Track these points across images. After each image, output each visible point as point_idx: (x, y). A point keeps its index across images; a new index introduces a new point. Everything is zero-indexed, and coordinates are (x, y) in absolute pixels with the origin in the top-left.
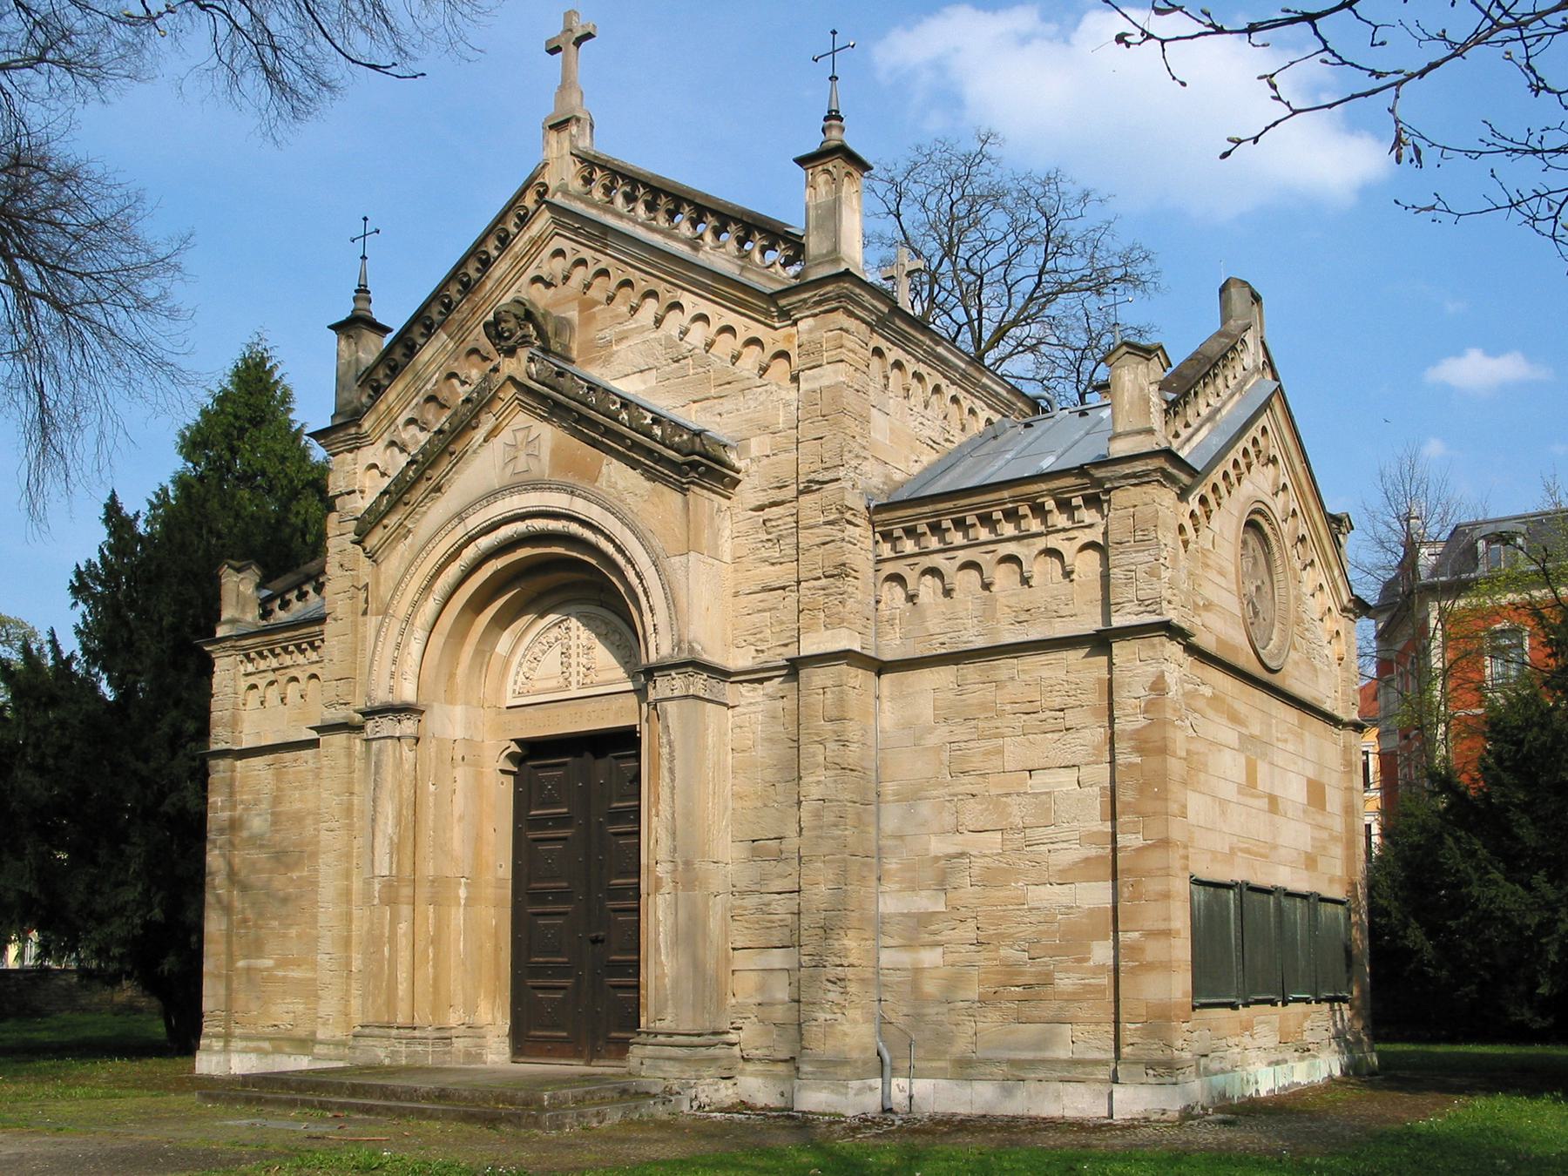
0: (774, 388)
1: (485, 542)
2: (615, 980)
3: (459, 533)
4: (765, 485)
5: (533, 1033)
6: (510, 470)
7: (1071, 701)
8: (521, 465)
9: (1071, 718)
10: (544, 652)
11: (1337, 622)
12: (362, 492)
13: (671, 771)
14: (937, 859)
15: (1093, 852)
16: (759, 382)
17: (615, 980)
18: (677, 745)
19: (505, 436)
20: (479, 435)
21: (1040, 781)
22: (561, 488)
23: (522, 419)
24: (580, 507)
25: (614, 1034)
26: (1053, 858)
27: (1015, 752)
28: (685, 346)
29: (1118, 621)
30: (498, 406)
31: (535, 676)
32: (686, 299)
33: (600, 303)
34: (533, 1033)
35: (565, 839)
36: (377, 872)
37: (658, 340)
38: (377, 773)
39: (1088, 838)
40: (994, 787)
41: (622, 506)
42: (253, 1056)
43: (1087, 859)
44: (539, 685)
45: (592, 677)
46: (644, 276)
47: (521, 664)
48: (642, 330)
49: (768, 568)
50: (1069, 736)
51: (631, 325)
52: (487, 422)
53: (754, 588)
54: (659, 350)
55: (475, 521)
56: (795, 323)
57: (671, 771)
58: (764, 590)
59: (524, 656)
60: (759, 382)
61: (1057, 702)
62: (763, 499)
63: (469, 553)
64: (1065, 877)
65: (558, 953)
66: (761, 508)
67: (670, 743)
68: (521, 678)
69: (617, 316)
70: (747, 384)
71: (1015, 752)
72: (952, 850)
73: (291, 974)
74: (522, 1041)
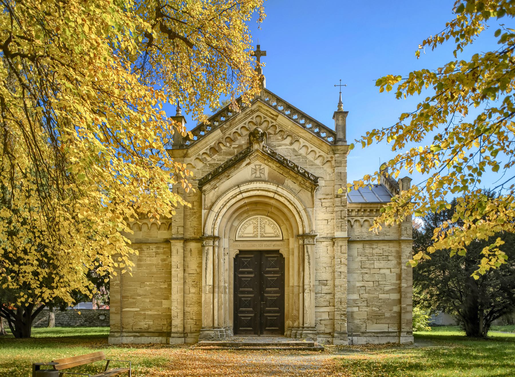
7: (390, 254)
8: (258, 175)
9: (390, 258)
11: (160, 232)
13: (309, 262)
14: (358, 287)
15: (394, 287)
16: (321, 167)
18: (311, 256)
19: (252, 166)
20: (244, 164)
21: (382, 271)
25: (267, 328)
26: (385, 288)
27: (377, 265)
29: (402, 238)
34: (267, 328)
36: (207, 284)
37: (291, 149)
38: (207, 255)
39: (394, 284)
40: (373, 271)
41: (287, 193)
42: (132, 338)
43: (392, 289)
48: (286, 145)
50: (389, 262)
52: (247, 161)
54: (291, 152)
55: (243, 188)
57: (309, 262)
60: (321, 167)
61: (387, 254)
64: (388, 292)
67: (309, 255)
69: (278, 139)
71: (377, 265)
72: (361, 285)
73: (147, 313)
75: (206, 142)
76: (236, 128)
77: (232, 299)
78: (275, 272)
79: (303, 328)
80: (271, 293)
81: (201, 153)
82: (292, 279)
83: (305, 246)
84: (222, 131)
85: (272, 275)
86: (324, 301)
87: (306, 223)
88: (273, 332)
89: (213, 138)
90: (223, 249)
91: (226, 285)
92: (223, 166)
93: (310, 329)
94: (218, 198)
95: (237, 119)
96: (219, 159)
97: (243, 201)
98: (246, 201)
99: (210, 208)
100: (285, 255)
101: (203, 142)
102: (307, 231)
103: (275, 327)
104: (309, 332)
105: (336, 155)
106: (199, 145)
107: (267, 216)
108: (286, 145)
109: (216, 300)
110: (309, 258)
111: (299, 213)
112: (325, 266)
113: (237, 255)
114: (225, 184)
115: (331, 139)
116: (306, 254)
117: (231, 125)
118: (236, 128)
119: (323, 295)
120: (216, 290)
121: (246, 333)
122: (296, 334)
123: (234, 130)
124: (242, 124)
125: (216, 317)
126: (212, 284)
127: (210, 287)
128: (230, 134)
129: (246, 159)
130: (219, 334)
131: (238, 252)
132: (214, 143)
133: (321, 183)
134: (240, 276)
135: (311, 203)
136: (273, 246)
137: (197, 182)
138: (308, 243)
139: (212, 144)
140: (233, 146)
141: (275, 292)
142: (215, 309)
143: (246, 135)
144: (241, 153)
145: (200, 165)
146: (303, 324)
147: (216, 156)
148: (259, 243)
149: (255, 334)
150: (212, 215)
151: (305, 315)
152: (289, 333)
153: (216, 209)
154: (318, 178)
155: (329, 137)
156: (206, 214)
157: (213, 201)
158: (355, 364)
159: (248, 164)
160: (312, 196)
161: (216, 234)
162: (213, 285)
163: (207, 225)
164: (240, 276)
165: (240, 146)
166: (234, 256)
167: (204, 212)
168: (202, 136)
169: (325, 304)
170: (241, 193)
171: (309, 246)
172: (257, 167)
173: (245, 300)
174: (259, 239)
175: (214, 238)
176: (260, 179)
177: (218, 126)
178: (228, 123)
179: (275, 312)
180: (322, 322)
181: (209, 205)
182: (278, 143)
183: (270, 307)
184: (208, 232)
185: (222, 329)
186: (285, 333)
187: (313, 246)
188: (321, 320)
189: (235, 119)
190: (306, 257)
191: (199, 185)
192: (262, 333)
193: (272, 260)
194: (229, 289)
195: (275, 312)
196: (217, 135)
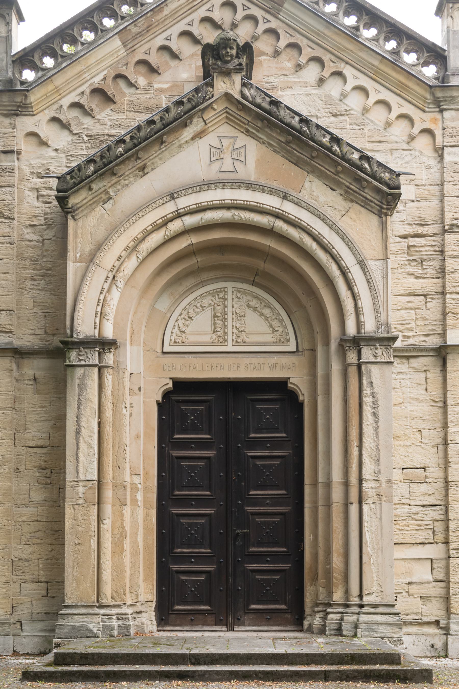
0: (417, 154)
1: (190, 221)
2: (255, 566)
3: (169, 208)
4: (410, 220)
5: (176, 608)
6: (211, 167)
8: (228, 165)
10: (197, 314)
12: (19, 153)
16: (406, 147)
17: (255, 566)
18: (380, 397)
19: (211, 139)
20: (188, 133)
22: (272, 192)
23: (226, 130)
24: (289, 208)
28: (342, 108)
30: (209, 115)
31: (188, 331)
32: (348, 71)
33: (267, 54)
35: (208, 458)
41: (318, 209)
44: (192, 338)
45: (243, 337)
46: (310, 44)
47: (177, 320)
48: (305, 85)
49: (412, 280)
51: (293, 79)
52: (197, 125)
53: (403, 292)
54: (320, 104)
55: (184, 202)
56: (441, 111)
57: (375, 415)
58: (410, 295)
59: (181, 314)
60: (406, 147)
62: (410, 230)
63: (176, 226)
65: (201, 545)
66: (405, 237)
67: (373, 395)
68: (176, 330)
69: (282, 69)
70: (395, 146)
74: (167, 612)
75: (80, 74)
76: (165, 35)
77: (154, 520)
78: (276, 444)
79: (361, 606)
80: (264, 501)
81: (66, 102)
82: (326, 462)
83: (363, 367)
84: (124, 44)
85: (266, 453)
86: (419, 528)
87: (366, 302)
88: (267, 618)
89: (99, 62)
90: (127, 374)
91: (136, 480)
92: (127, 138)
93: (381, 610)
94: (115, 230)
95: (166, 11)
96: (114, 122)
97: (186, 237)
98: (195, 239)
99: (91, 259)
100: (304, 396)
101: (70, 73)
102: (369, 327)
103: (276, 602)
104: (379, 618)
105: (447, 114)
106: (59, 80)
107: (253, 283)
108: (305, 85)
109: (107, 524)
110: (375, 405)
111: (344, 273)
112: (420, 426)
113: (167, 395)
114: (135, 191)
115: (430, 71)
116: (367, 391)
117: (148, 29)
118: (165, 35)
119: (415, 509)
120: (108, 494)
121: (192, 619)
122: (340, 625)
123: (159, 41)
124: (182, 26)
125: (107, 576)
126: (96, 478)
127: (90, 484)
128: (148, 53)
129: (195, 120)
130: (115, 623)
131: (170, 385)
132: (101, 76)
133: (407, 191)
134: (175, 454)
135: (379, 247)
136: (271, 368)
137: (54, 183)
138: (372, 359)
139: (97, 79)
140: (156, 86)
141: (276, 501)
142: (103, 550)
143: (192, 55)
144: (179, 103)
145: (59, 139)
146: (361, 596)
147: (106, 115)
148: (231, 359)
149: (219, 623)
150: (97, 278)
151: (365, 568)
152: (317, 621)
153: (108, 258)
154: (399, 175)
155: (426, 64)
156: (79, 275)
157: (100, 237)
158: (138, 528)
159: (199, 135)
160: (384, 227)
161: (109, 332)
162: (99, 481)
163: (82, 298)
164: (175, 454)
165: (176, 85)
166: (159, 398)
167: (72, 269)
168: (65, 57)
169: (422, 536)
170: (178, 215)
171: (375, 369)
172: (226, 142)
173: (190, 525)
174: (230, 348)
175: (105, 345)
176: (232, 176)
177: (115, 27)
178: (142, 23)
179: (276, 558)
180: (413, 589)
181: (87, 249)
182: (283, 79)
183: (258, 547)
184: (85, 328)
185: (124, 610)
186: (306, 623)
187: (385, 367)
188: (409, 583)
189: (162, 10)
190: (368, 400)
191: (59, 191)
192: (239, 622)
193: (266, 410)
194: (146, 490)
195: (276, 558)
196: (111, 54)
